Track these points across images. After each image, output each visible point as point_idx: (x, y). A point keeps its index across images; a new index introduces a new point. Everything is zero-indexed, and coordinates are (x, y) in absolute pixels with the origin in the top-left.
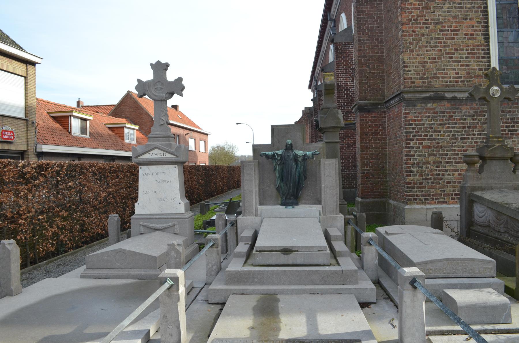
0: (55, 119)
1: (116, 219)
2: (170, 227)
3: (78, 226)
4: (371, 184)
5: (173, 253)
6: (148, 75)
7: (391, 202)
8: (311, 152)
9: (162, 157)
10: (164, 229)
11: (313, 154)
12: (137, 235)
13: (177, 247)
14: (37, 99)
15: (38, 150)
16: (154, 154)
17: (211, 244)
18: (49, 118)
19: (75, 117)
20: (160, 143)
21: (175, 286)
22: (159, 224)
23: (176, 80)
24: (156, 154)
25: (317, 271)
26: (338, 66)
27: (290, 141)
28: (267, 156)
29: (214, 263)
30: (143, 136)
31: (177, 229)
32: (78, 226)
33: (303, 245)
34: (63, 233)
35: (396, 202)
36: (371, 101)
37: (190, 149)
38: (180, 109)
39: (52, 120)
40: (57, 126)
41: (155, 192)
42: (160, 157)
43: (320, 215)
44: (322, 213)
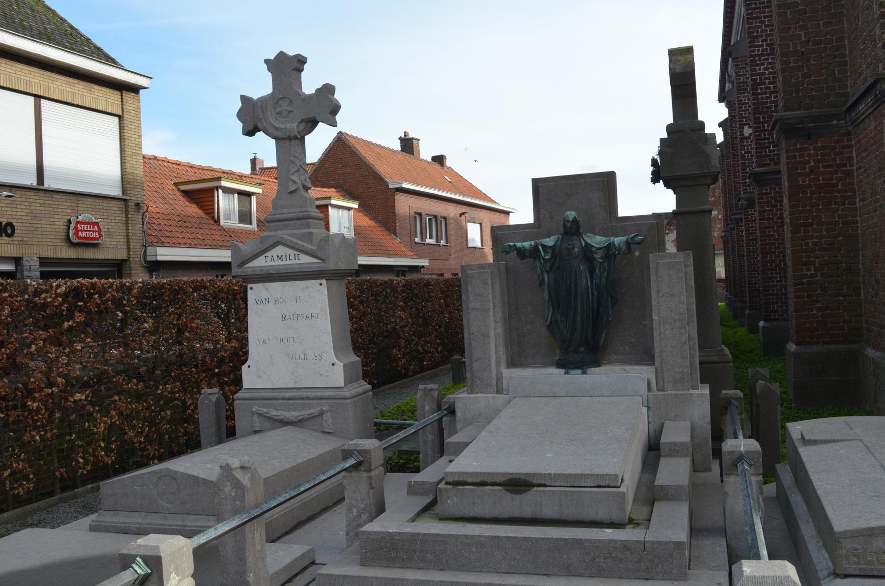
0: (189, 195)
1: (214, 398)
2: (312, 418)
3: (168, 412)
4: (819, 309)
5: (228, 488)
6: (262, 86)
7: (871, 352)
8: (623, 239)
9: (293, 262)
10: (301, 421)
11: (628, 243)
12: (249, 435)
13: (238, 474)
14: (144, 157)
15: (149, 259)
16: (276, 258)
17: (352, 462)
18: (178, 193)
19: (228, 191)
20: (290, 232)
21: (154, 579)
22: (296, 410)
23: (318, 90)
24: (280, 258)
25: (578, 542)
26: (753, 39)
27: (571, 215)
28: (522, 253)
29: (362, 506)
30: (374, 224)
31: (328, 421)
32: (168, 412)
33: (559, 472)
34: (133, 427)
35: (878, 354)
36: (814, 110)
37: (470, 245)
38: (449, 163)
39: (182, 199)
40: (193, 210)
41: (282, 340)
42: (289, 262)
43: (649, 389)
44: (654, 385)
